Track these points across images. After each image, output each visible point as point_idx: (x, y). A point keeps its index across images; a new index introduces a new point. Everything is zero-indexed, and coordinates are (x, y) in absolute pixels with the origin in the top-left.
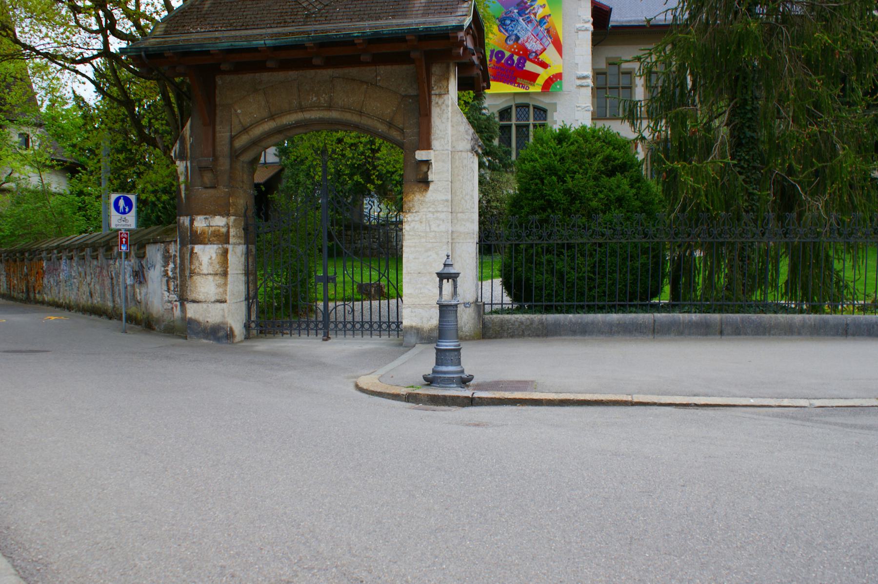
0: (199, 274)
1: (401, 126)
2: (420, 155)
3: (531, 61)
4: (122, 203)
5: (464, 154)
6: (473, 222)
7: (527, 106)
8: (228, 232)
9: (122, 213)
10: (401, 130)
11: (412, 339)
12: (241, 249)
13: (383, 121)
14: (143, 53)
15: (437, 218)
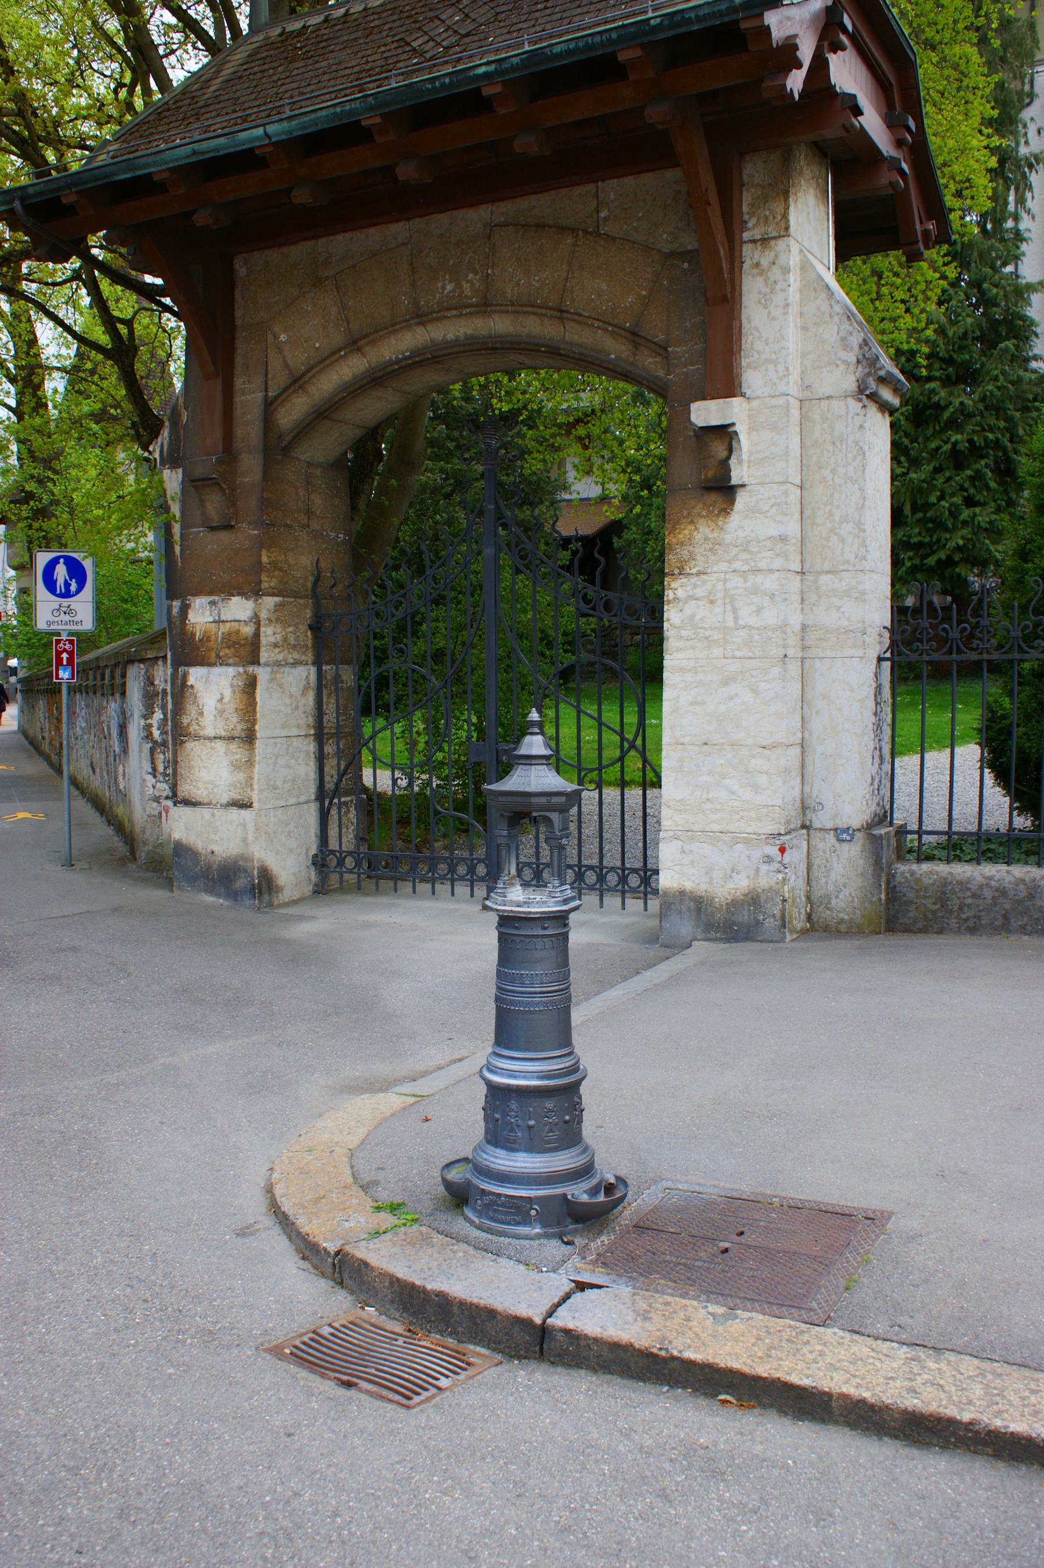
0: (197, 737)
1: (661, 337)
2: (705, 413)
4: (61, 572)
5: (837, 406)
6: (861, 598)
8: (257, 634)
9: (61, 596)
10: (662, 349)
11: (683, 927)
12: (300, 677)
13: (617, 330)
14: (17, 204)
15: (755, 591)
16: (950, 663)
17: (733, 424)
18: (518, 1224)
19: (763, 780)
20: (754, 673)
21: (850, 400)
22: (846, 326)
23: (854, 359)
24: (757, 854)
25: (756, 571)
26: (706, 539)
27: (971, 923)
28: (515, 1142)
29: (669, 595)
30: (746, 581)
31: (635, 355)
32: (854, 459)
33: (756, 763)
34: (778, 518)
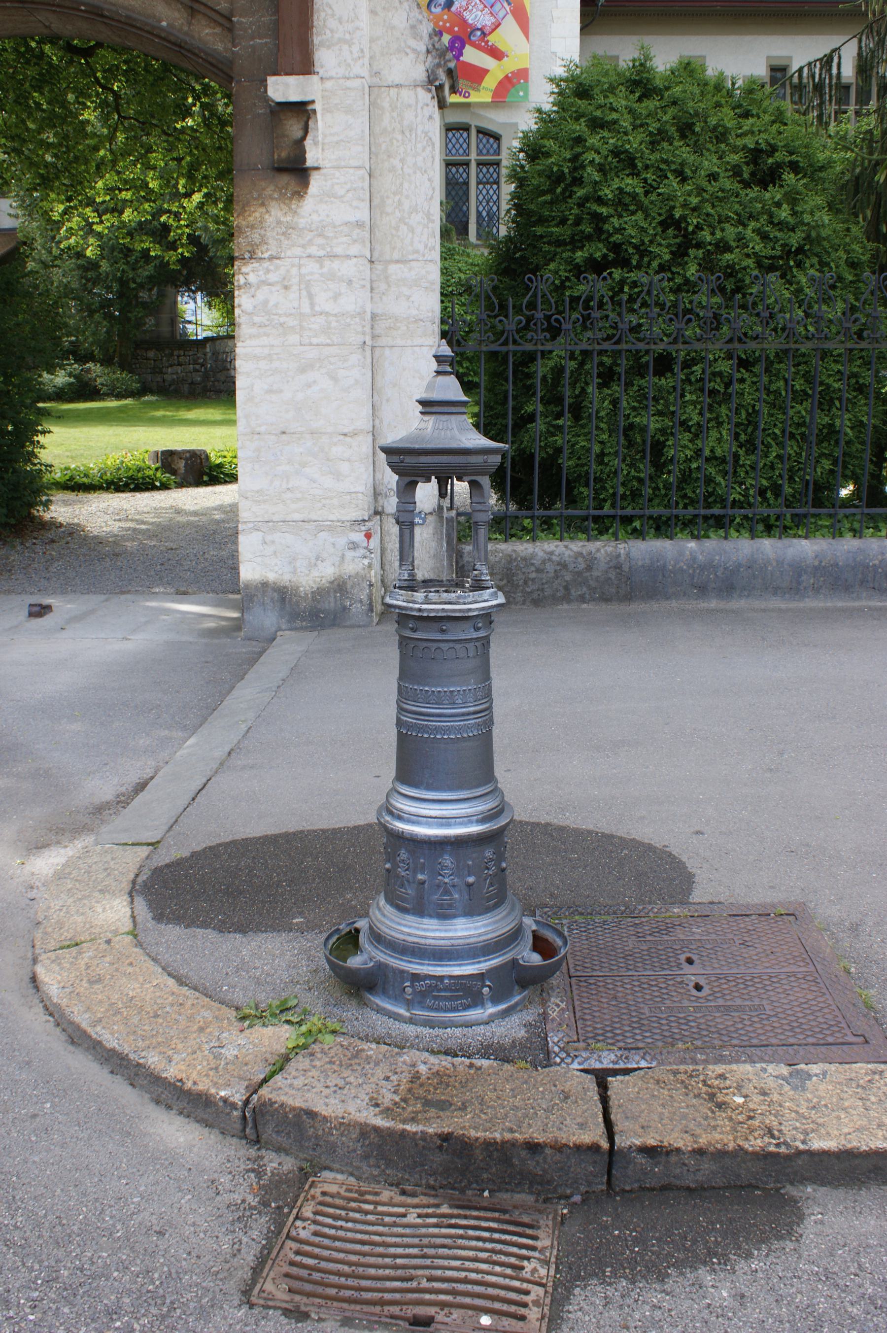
2: (282, 88)
3: (473, 45)
5: (407, 95)
7: (466, 128)
11: (267, 618)
15: (332, 277)
16: (536, 351)
17: (313, 102)
18: (467, 1007)
19: (345, 467)
20: (331, 359)
21: (419, 90)
22: (416, 13)
23: (424, 49)
24: (342, 541)
25: (333, 256)
26: (279, 222)
27: (535, 596)
28: (450, 906)
29: (240, 280)
30: (322, 267)
31: (190, 24)
32: (424, 149)
33: (337, 451)
34: (355, 203)
